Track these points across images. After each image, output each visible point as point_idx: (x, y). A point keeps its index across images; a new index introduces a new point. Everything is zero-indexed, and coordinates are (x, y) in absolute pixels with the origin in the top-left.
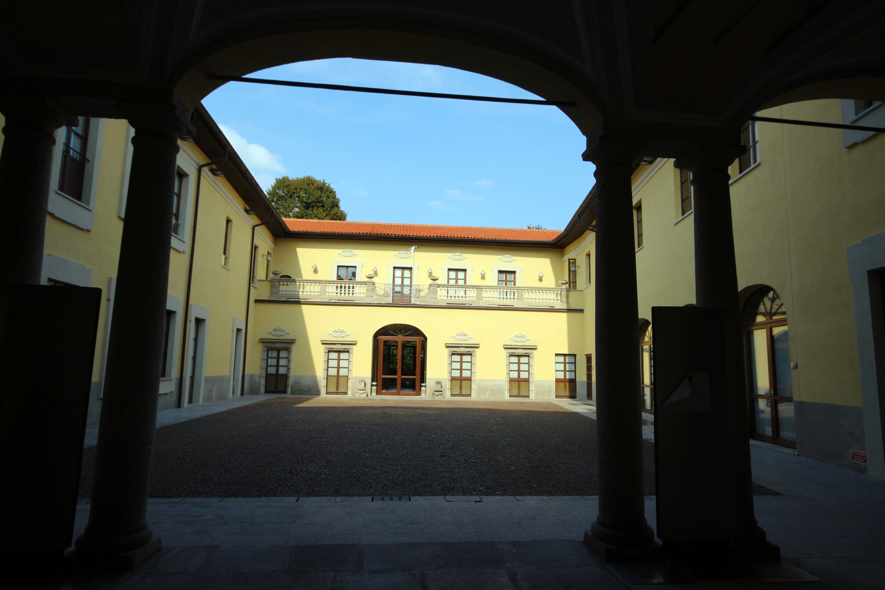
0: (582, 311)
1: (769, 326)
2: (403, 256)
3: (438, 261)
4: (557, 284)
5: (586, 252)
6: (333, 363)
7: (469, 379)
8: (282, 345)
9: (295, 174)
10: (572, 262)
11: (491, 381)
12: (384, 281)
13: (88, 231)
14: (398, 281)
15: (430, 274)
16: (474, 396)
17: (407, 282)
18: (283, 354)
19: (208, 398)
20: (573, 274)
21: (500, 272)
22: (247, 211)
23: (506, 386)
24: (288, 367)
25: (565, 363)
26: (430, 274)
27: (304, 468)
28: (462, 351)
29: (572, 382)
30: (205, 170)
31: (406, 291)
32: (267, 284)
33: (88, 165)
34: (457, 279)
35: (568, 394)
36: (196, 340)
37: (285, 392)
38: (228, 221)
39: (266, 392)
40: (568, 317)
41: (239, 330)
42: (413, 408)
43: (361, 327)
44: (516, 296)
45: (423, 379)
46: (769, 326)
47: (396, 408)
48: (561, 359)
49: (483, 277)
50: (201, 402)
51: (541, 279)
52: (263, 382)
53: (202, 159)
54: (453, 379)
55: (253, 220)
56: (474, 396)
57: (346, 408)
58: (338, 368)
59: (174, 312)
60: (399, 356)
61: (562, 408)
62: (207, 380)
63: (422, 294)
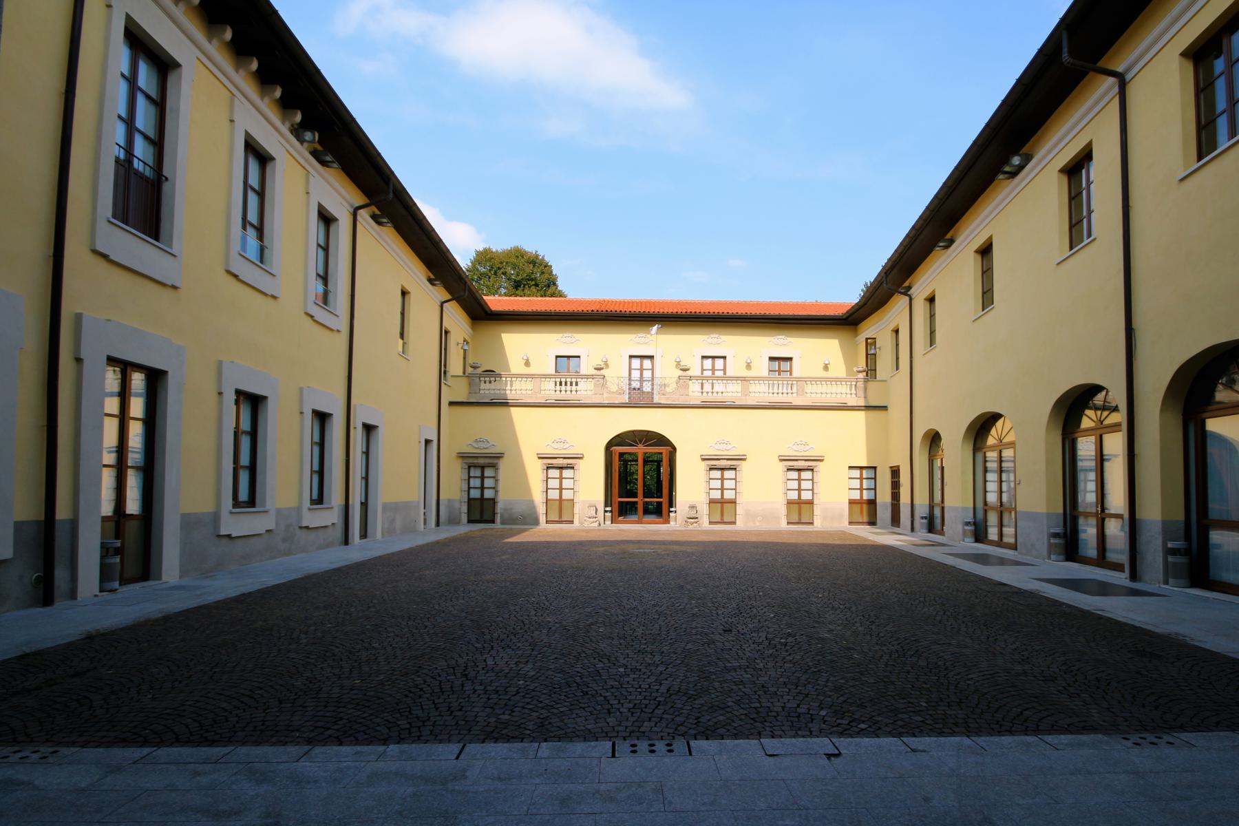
0: (885, 408)
1: (1098, 432)
2: (642, 340)
3: (688, 347)
4: (848, 374)
5: (892, 326)
6: (554, 483)
7: (733, 502)
8: (487, 461)
9: (500, 245)
10: (871, 343)
11: (761, 506)
12: (618, 375)
13: (174, 287)
14: (636, 374)
15: (678, 363)
16: (741, 524)
17: (647, 374)
18: (488, 472)
19: (389, 531)
20: (871, 359)
21: (772, 359)
22: (430, 281)
23: (782, 510)
24: (495, 488)
25: (861, 479)
26: (678, 363)
27: (490, 662)
28: (722, 466)
29: (872, 503)
30: (364, 215)
31: (647, 387)
32: (464, 382)
33: (166, 187)
34: (713, 370)
35: (865, 519)
36: (367, 453)
37: (493, 521)
38: (404, 293)
39: (470, 521)
40: (867, 418)
41: (427, 442)
42: (663, 543)
43: (589, 436)
44: (795, 390)
45: (671, 503)
46: (1098, 432)
47: (639, 542)
48: (857, 473)
49: (749, 366)
50: (379, 536)
51: (826, 368)
52: (465, 509)
53: (358, 199)
54: (712, 502)
55: (440, 293)
56: (741, 524)
57: (571, 543)
58: (561, 489)
59: (330, 415)
60: (640, 474)
61: (866, 539)
62: (386, 507)
63: (668, 390)
